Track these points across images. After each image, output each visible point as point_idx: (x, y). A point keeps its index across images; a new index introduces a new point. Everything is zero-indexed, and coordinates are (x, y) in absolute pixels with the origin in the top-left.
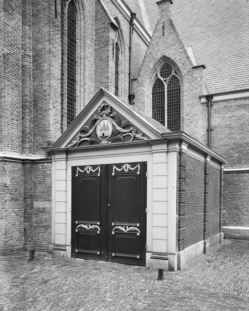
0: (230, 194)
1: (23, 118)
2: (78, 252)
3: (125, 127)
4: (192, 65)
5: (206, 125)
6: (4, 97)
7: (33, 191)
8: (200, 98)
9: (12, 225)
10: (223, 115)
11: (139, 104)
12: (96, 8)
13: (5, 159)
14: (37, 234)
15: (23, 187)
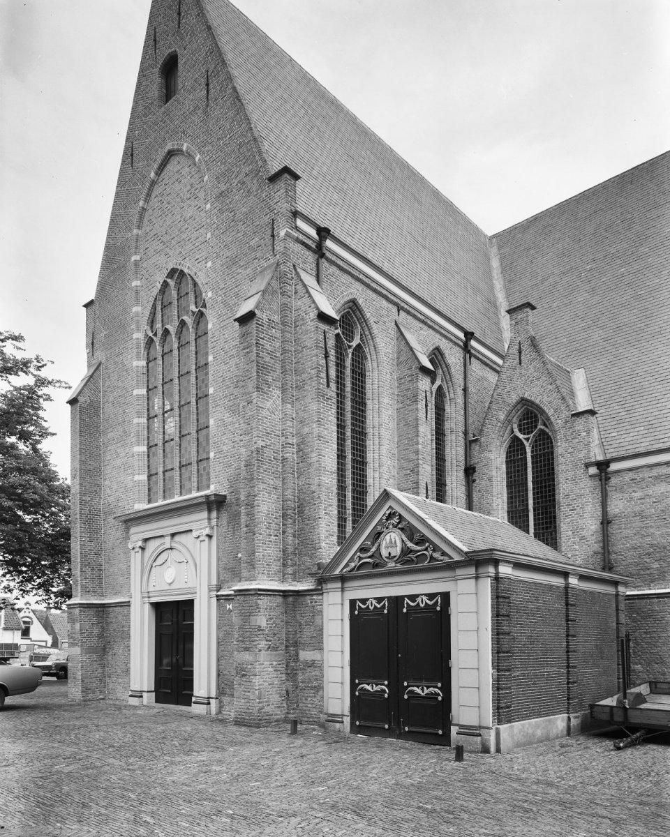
0: (648, 636)
1: (284, 532)
2: (359, 726)
3: (419, 543)
4: (572, 411)
5: (600, 513)
6: (258, 506)
7: (298, 636)
8: (588, 466)
9: (269, 685)
10: (629, 494)
11: (483, 482)
12: (398, 346)
13: (259, 592)
14: (304, 699)
15: (284, 630)
